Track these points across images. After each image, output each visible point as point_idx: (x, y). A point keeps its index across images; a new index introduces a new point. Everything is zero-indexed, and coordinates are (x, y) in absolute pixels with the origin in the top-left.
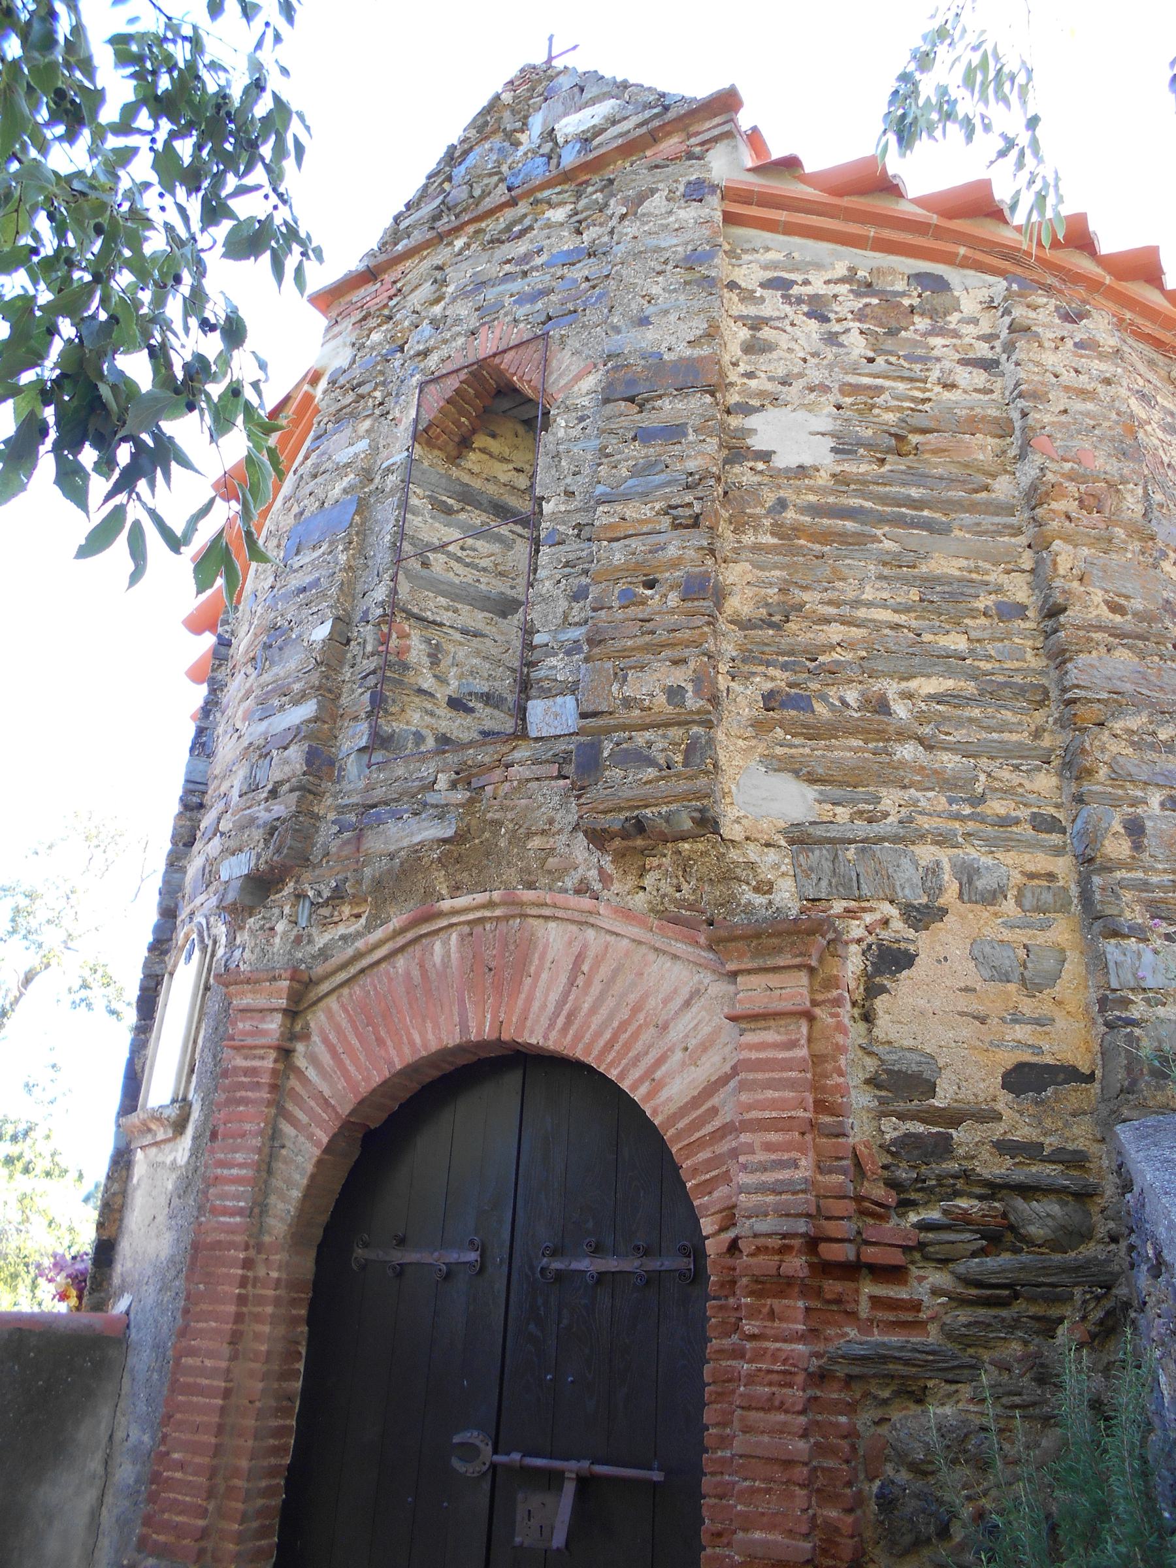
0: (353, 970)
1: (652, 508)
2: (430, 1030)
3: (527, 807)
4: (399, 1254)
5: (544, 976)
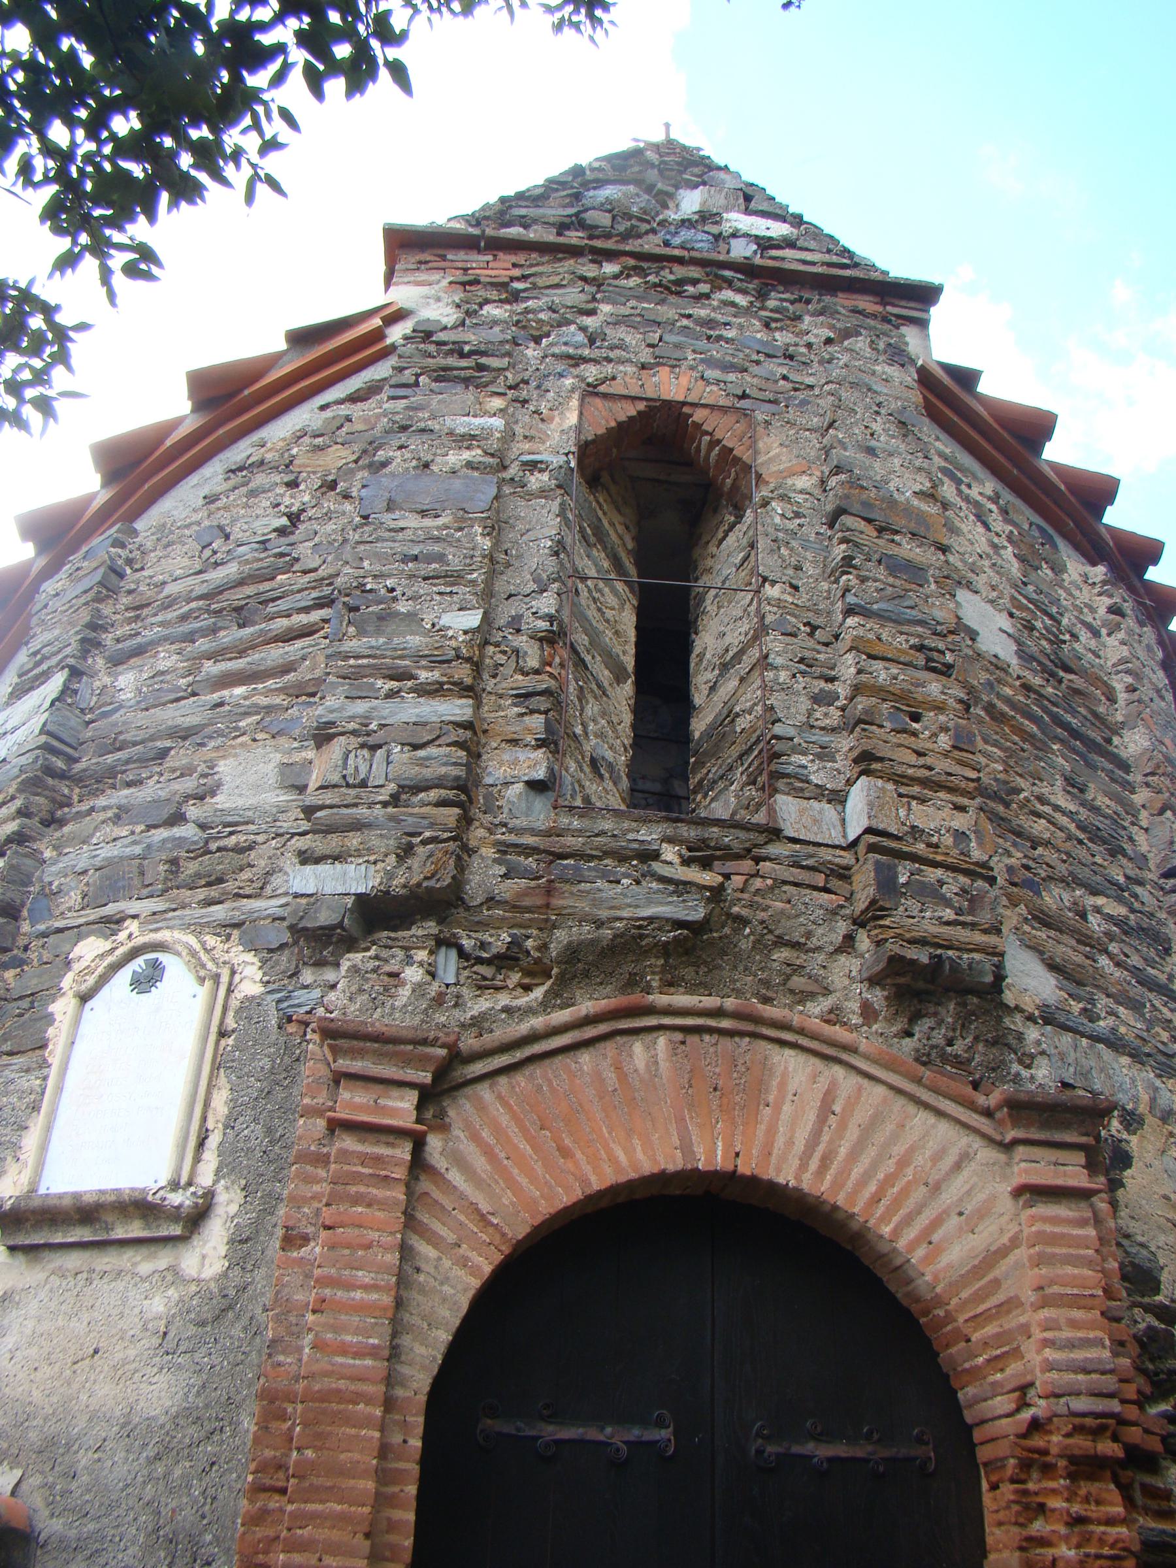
0: (519, 1055)
1: (907, 641)
3: (782, 912)
5: (787, 1108)
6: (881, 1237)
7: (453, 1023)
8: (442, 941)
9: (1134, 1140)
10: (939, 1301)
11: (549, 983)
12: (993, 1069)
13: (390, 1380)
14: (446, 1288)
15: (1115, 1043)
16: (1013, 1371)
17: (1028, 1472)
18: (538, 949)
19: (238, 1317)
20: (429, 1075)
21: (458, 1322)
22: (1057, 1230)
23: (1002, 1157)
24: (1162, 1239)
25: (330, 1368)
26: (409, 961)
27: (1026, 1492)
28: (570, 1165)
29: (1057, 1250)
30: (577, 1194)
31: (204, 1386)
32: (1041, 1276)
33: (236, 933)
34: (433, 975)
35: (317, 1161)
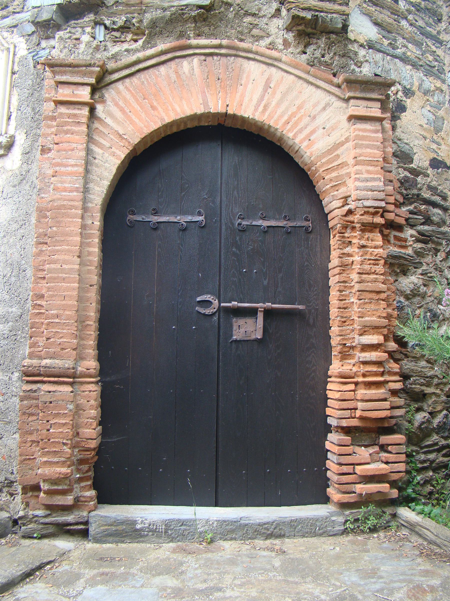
0: (134, 69)
2: (185, 105)
4: (156, 218)
5: (250, 86)
6: (289, 138)
7: (104, 58)
8: (97, 23)
9: (408, 101)
10: (313, 164)
11: (145, 38)
12: (342, 68)
13: (85, 200)
14: (106, 164)
15: (404, 59)
16: (342, 191)
17: (346, 230)
18: (138, 22)
19: (27, 182)
20: (94, 80)
21: (112, 177)
22: (365, 134)
23: (344, 105)
24: (416, 142)
25: (60, 197)
26: (84, 32)
27: (343, 237)
28: (156, 113)
29: (364, 142)
30: (159, 124)
31: (17, 209)
32: (356, 153)
33: (15, 30)
34: (94, 38)
35: (52, 119)
